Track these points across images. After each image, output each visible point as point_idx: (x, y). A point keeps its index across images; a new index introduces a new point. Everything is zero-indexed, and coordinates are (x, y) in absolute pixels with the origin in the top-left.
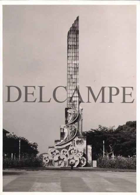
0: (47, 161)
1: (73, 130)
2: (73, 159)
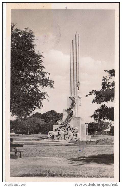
0: (50, 135)
1: (71, 113)
2: (67, 134)
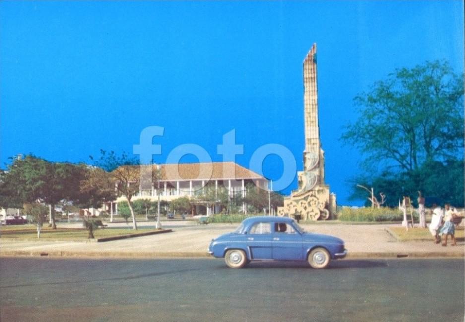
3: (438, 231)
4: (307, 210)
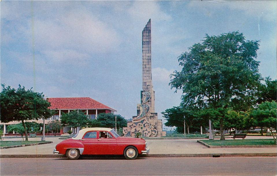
0: (126, 132)
3: (233, 138)
4: (143, 130)
